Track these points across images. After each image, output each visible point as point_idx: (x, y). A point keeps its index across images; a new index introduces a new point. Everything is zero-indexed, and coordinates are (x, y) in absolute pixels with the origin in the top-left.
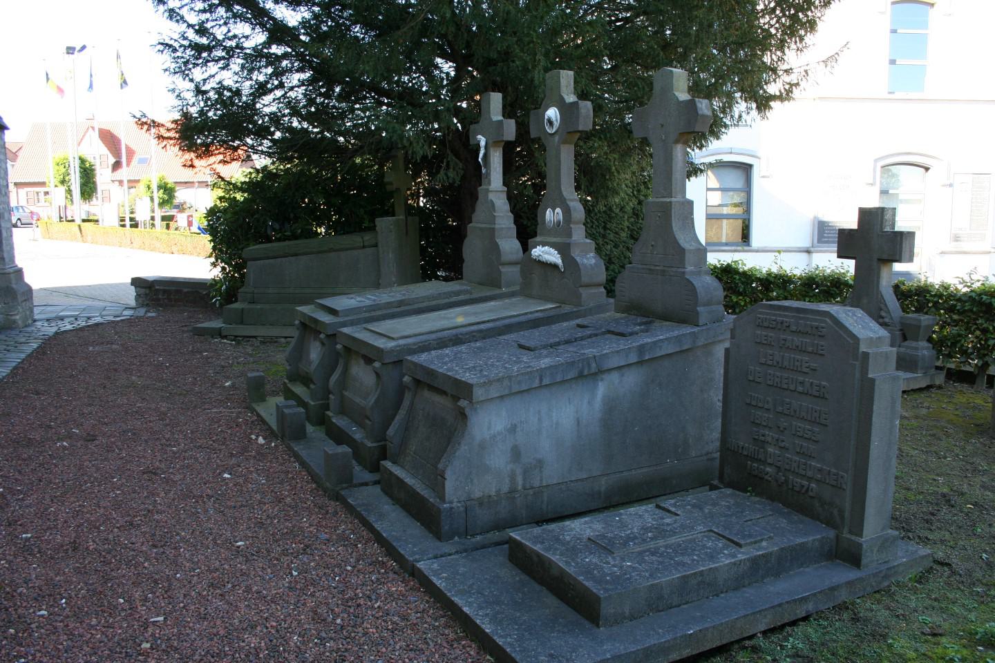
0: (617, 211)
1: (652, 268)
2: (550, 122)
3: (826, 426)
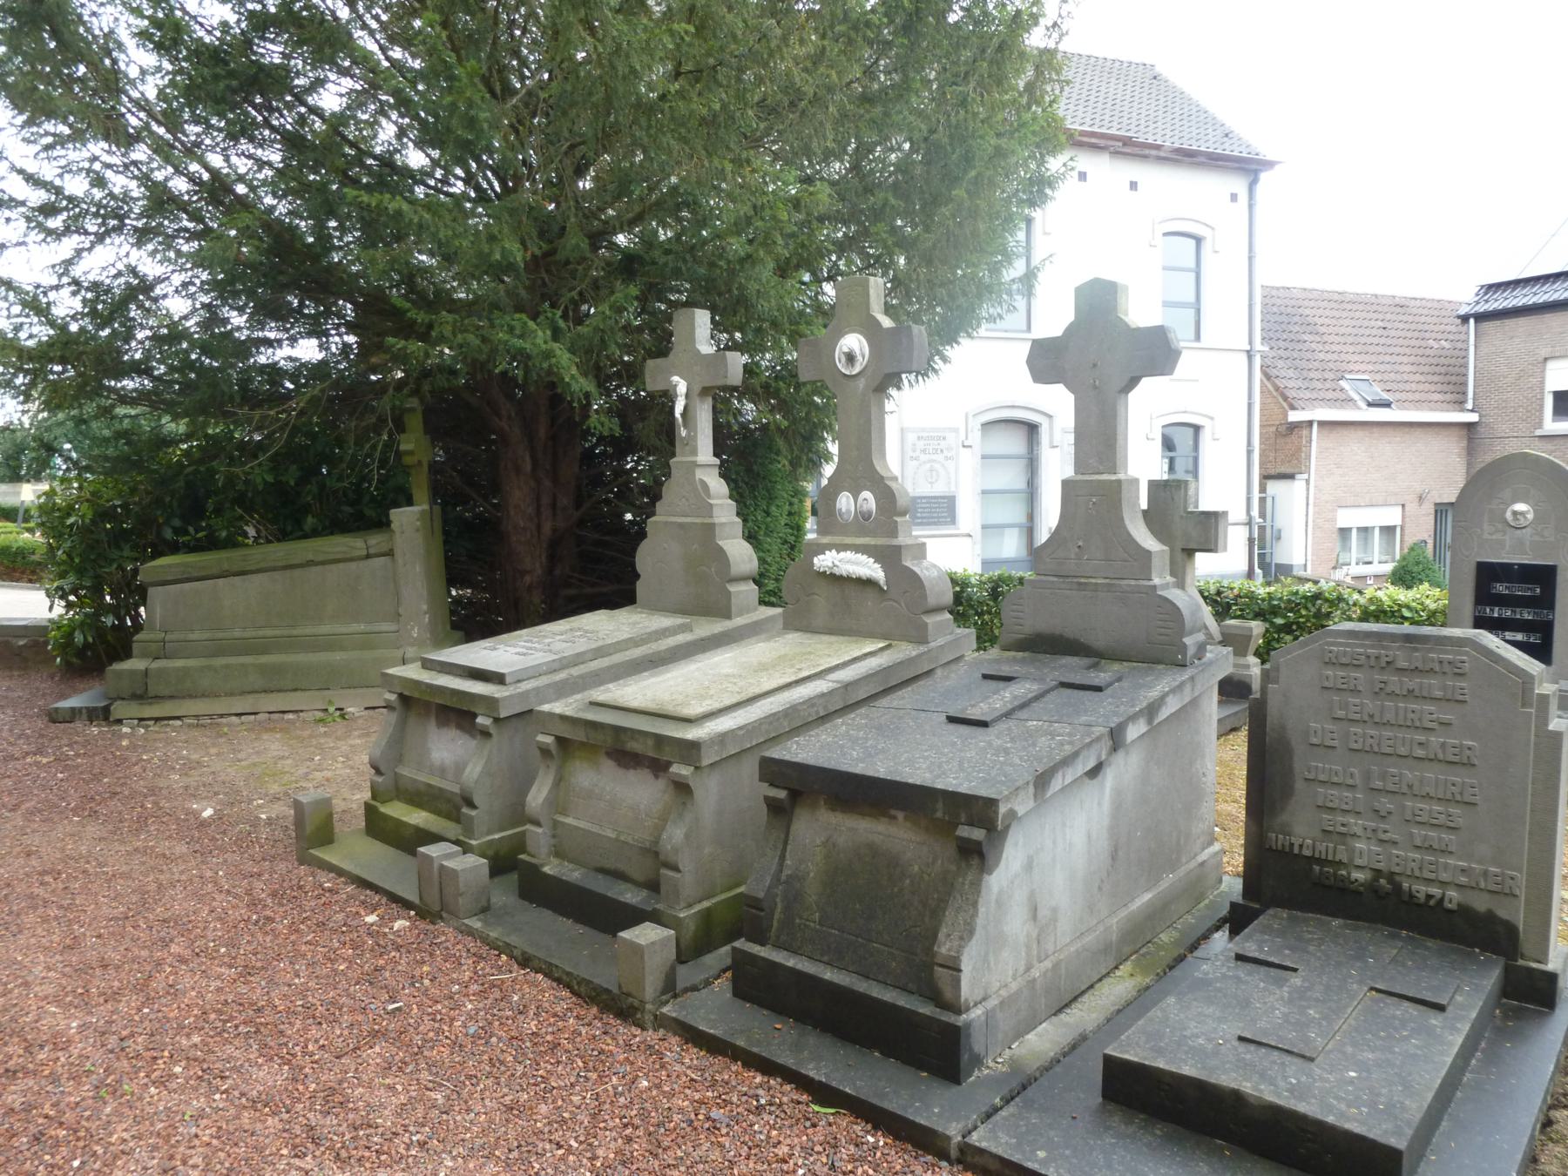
1: (1083, 580)
2: (850, 358)
3: (1475, 804)
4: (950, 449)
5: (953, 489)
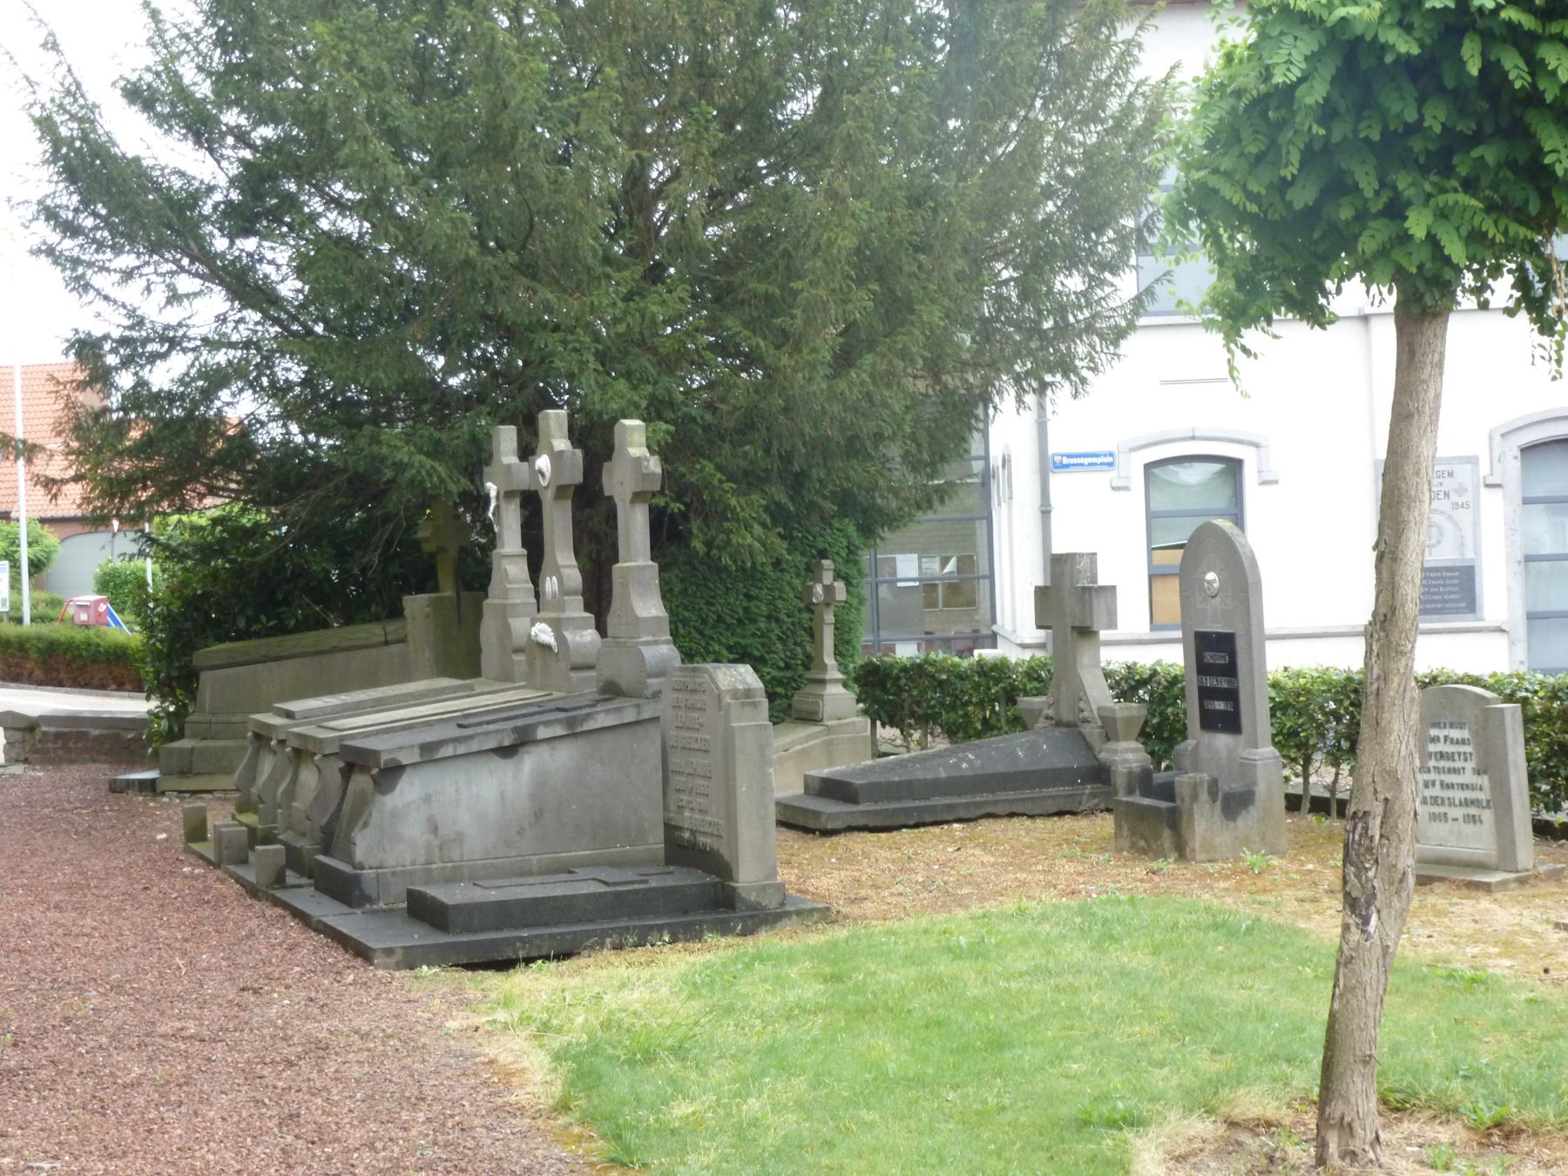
0: (768, 569)
4: (1461, 490)
5: (1470, 555)
